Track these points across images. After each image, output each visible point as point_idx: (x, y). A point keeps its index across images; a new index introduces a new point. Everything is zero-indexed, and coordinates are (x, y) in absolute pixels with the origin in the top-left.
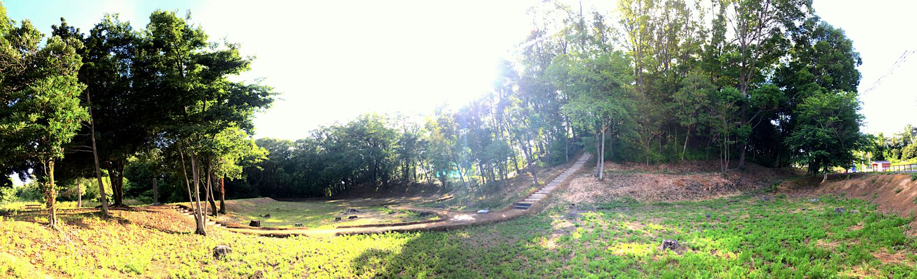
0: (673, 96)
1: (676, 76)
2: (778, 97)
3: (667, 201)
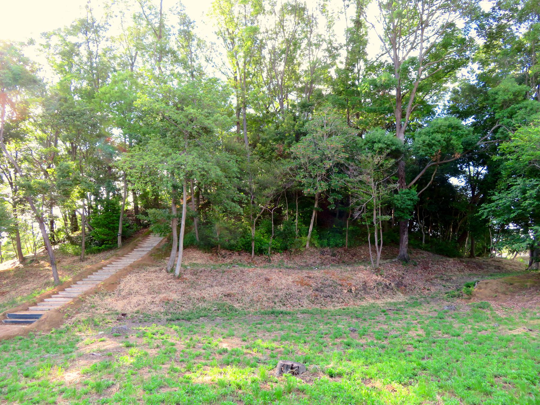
0: (292, 149)
1: (295, 119)
2: (460, 136)
3: (283, 309)
